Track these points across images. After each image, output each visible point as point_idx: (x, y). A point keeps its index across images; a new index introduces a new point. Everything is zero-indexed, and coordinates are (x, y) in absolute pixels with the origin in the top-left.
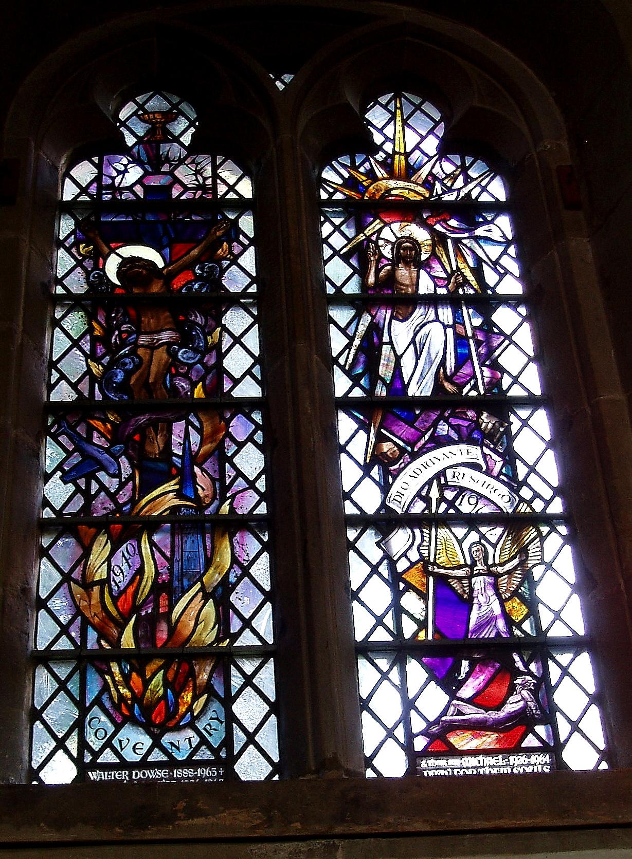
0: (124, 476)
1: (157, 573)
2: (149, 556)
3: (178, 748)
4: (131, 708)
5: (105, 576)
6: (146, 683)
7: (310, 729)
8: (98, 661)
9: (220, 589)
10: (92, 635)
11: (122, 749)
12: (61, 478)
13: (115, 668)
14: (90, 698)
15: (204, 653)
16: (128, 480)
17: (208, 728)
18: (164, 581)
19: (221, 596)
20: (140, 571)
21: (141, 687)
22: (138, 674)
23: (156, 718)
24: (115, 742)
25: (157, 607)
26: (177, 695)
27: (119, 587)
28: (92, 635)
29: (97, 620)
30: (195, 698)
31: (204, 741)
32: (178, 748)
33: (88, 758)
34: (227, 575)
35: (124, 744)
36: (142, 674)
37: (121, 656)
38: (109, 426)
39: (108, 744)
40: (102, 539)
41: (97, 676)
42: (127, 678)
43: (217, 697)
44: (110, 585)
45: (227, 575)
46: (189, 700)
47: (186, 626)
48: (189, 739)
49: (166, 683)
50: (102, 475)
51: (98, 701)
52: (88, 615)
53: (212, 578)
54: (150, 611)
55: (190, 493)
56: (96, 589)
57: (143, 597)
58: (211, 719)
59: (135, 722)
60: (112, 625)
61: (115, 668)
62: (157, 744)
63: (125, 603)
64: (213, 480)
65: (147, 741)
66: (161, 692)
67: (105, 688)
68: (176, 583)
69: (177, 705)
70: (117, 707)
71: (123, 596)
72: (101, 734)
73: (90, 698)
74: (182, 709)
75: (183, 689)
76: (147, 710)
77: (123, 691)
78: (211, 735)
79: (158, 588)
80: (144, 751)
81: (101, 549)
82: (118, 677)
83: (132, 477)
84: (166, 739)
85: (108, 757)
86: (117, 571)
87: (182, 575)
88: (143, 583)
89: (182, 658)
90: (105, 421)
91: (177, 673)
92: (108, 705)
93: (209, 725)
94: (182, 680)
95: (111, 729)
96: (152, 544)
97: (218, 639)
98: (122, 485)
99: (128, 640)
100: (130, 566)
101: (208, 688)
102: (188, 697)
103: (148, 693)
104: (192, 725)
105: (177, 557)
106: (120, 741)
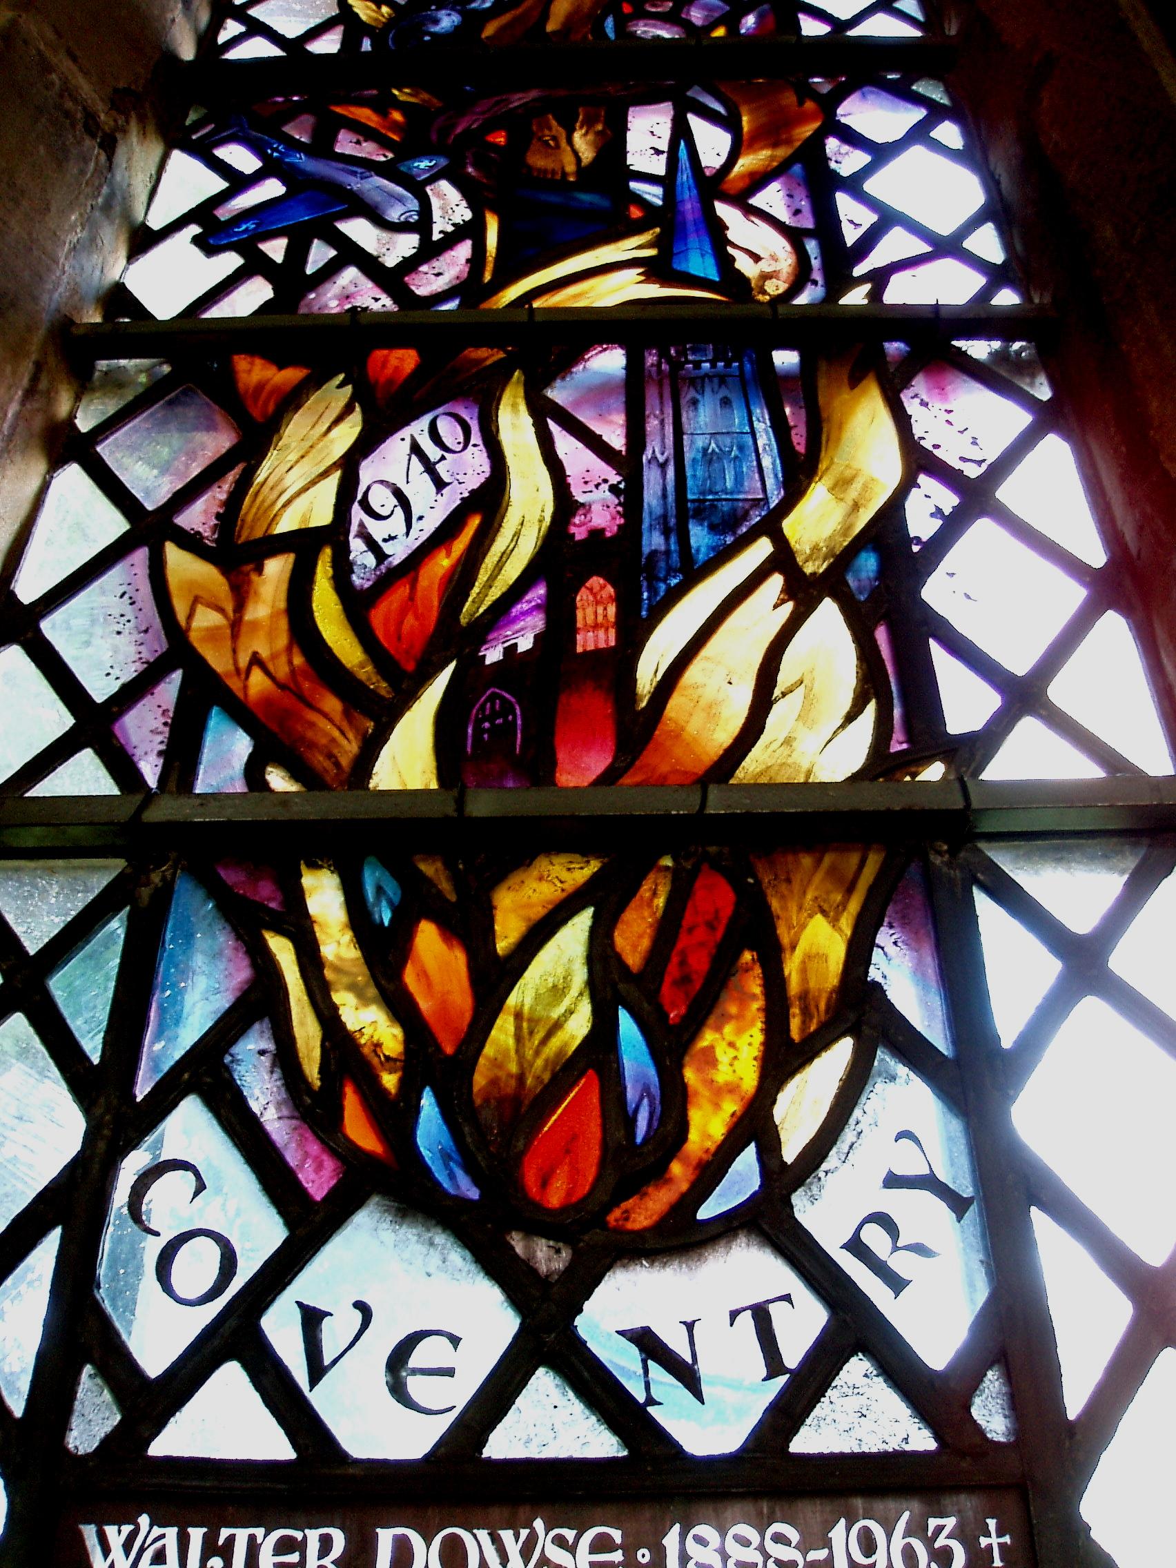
0: (440, 226)
1: (565, 504)
2: (540, 470)
3: (687, 1376)
4: (396, 1118)
5: (323, 516)
6: (494, 977)
7: (560, 1111)
8: (248, 867)
9: (868, 563)
10: (226, 753)
11: (317, 1371)
12: (196, 240)
13: (323, 895)
14: (164, 1049)
15: (807, 825)
16: (450, 241)
17: (875, 1238)
18: (596, 533)
19: (883, 588)
20: (489, 500)
21: (461, 997)
22: (451, 931)
23: (545, 1183)
24: (280, 1327)
25: (560, 617)
26: (673, 1046)
27: (381, 556)
28: (226, 753)
29: (258, 680)
30: (782, 1060)
31: (855, 1330)
32: (687, 1376)
33: (92, 1420)
34: (894, 509)
35: (333, 1337)
36: (469, 926)
37: (365, 837)
38: (397, 116)
39: (234, 1336)
40: (335, 394)
41: (224, 939)
42: (384, 953)
43: (913, 1050)
44: (341, 552)
45: (894, 509)
46: (749, 1077)
47: (712, 712)
48: (761, 1315)
49: (607, 980)
50: (359, 230)
51: (206, 1074)
52: (218, 660)
53: (816, 523)
54: (525, 643)
55: (700, 264)
56: (277, 569)
57: (495, 593)
58: (893, 1181)
59: (416, 1199)
60: (332, 704)
61: (323, 895)
62: (547, 1340)
63: (407, 618)
64: (794, 236)
65: (486, 1321)
66: (579, 1026)
67: (259, 1002)
68: (653, 541)
69: (674, 1101)
70: (314, 1108)
71: (400, 593)
72: (196, 1268)
73: (164, 1049)
74: (708, 1125)
75: (703, 1010)
76: (499, 1129)
77: (370, 1022)
78: (897, 1284)
79: (564, 558)
80: (458, 1393)
81: (316, 436)
82: (337, 944)
83: (472, 231)
84: (611, 1313)
85: (226, 1423)
86: (381, 499)
87: (684, 510)
88: (500, 544)
89: (711, 865)
90: (382, 105)
91: (667, 930)
92: (261, 1090)
93: (883, 1220)
94: (700, 964)
95: (260, 1232)
96: (542, 411)
97: (880, 763)
98: (429, 250)
99: (407, 759)
100: (440, 484)
101: (859, 1010)
102: (733, 1052)
103: (503, 1032)
104: (769, 1219)
105: (657, 446)
106: (312, 1319)
